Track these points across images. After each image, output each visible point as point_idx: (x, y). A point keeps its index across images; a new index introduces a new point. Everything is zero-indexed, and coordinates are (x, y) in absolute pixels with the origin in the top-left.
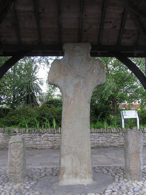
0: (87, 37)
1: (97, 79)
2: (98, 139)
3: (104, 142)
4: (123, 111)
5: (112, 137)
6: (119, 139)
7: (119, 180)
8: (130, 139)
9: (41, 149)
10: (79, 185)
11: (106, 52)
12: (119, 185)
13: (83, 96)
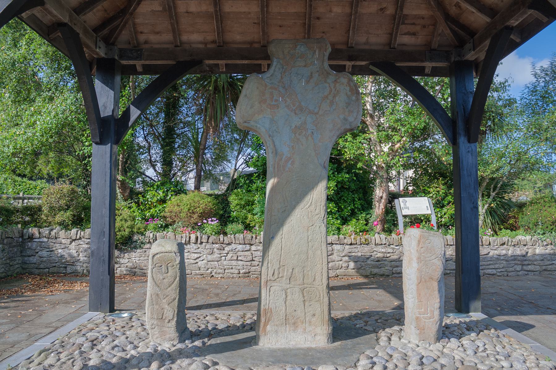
0: (323, 33)
1: (342, 117)
4: (401, 199)
11: (363, 63)
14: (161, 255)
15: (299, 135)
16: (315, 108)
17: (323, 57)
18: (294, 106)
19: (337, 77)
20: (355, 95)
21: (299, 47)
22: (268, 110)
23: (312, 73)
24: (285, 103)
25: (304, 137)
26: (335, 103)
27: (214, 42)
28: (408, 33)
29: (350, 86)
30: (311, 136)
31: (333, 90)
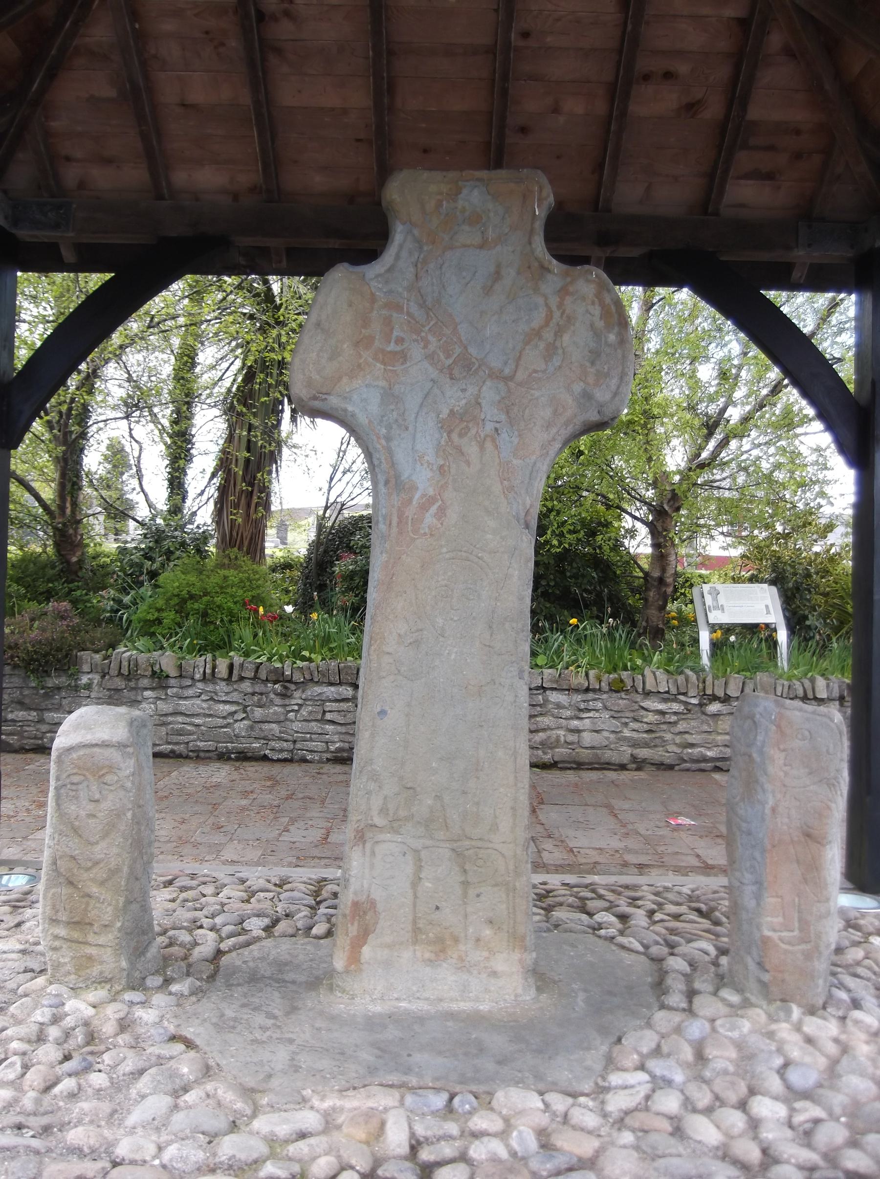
1: (578, 387)
2: (575, 723)
3: (607, 738)
5: (651, 718)
6: (682, 726)
7: (691, 994)
8: (773, 752)
9: (285, 760)
10: (452, 1016)
12: (696, 1029)
13: (497, 488)
14: (81, 752)
15: (461, 435)
16: (506, 363)
17: (532, 224)
18: (448, 357)
19: (569, 279)
20: (616, 329)
21: (465, 191)
22: (378, 365)
23: (499, 266)
24: (425, 347)
25: (473, 443)
26: (560, 351)
27: (253, 189)
28: (756, 175)
29: (603, 305)
30: (494, 440)
31: (557, 314)
